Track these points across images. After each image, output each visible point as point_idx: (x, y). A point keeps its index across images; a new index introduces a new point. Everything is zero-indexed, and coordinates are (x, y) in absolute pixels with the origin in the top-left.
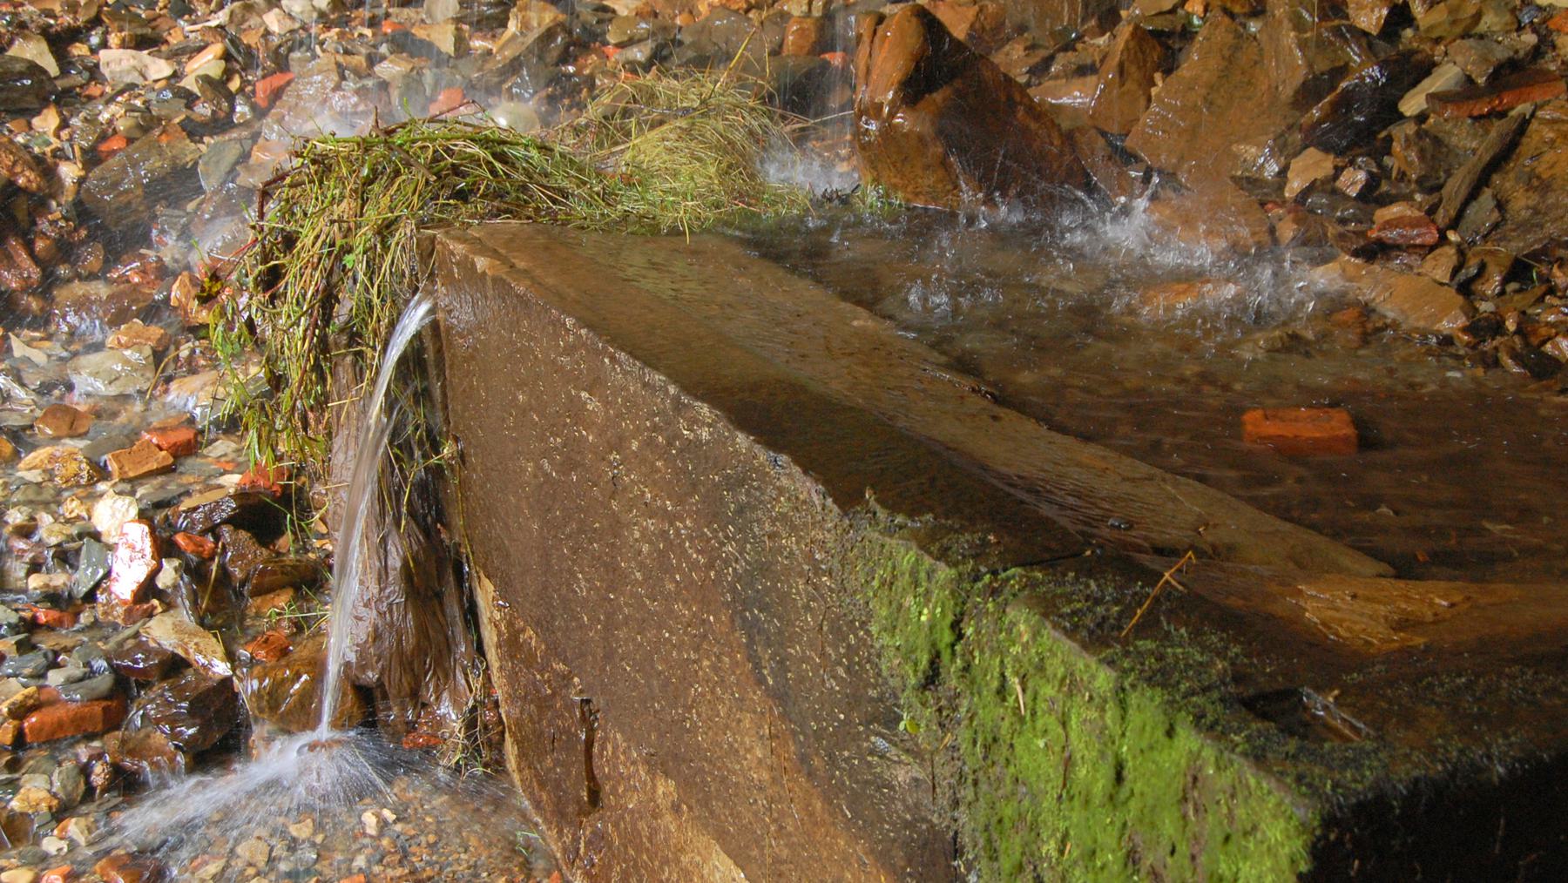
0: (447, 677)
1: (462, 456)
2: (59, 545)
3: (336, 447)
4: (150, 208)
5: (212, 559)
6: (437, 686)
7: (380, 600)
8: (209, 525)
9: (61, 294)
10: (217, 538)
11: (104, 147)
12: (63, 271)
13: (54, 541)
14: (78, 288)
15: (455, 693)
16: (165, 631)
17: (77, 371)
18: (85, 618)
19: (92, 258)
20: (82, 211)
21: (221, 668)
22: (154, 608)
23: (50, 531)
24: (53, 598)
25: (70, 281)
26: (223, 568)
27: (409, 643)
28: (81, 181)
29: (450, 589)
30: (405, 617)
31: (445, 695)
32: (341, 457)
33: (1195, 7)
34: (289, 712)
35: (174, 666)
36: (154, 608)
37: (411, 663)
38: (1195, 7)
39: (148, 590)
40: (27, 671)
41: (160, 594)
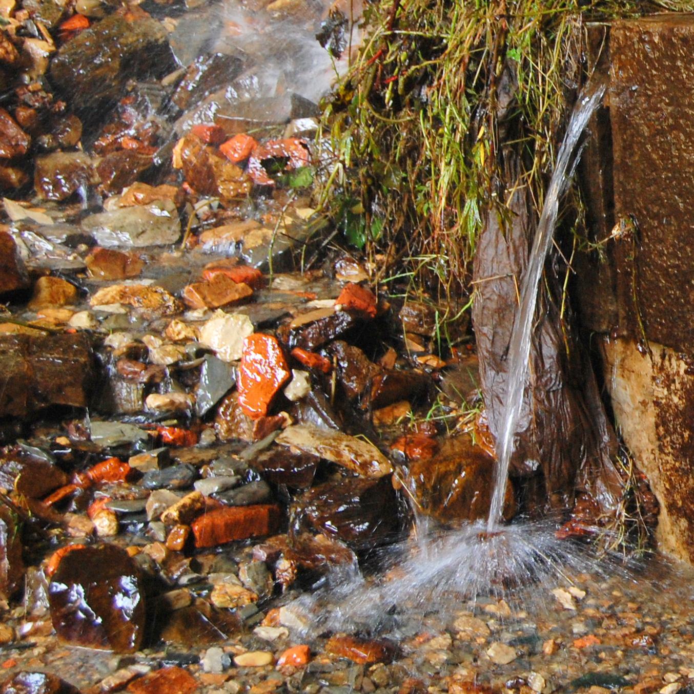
0: (597, 466)
1: (638, 235)
2: (176, 364)
3: (484, 242)
4: (124, 80)
5: (329, 374)
6: (590, 473)
7: (537, 388)
8: (322, 340)
9: (46, 163)
10: (331, 353)
11: (66, 26)
12: (46, 140)
13: (170, 360)
14: (63, 158)
15: (606, 478)
16: (306, 437)
17: (98, 225)
18: (206, 438)
19: (71, 132)
20: (57, 81)
21: (379, 468)
22: (284, 420)
23: (162, 354)
24: (177, 414)
25: (51, 150)
26: (339, 383)
27: (568, 429)
28: (52, 55)
29: (592, 382)
30: (562, 403)
31: (599, 482)
32: (491, 251)
33: (7, 330)
34: (452, 504)
35: (324, 471)
36: (284, 420)
37: (569, 451)
38: (7, 330)
39: (279, 402)
40: (175, 482)
41: (288, 406)
